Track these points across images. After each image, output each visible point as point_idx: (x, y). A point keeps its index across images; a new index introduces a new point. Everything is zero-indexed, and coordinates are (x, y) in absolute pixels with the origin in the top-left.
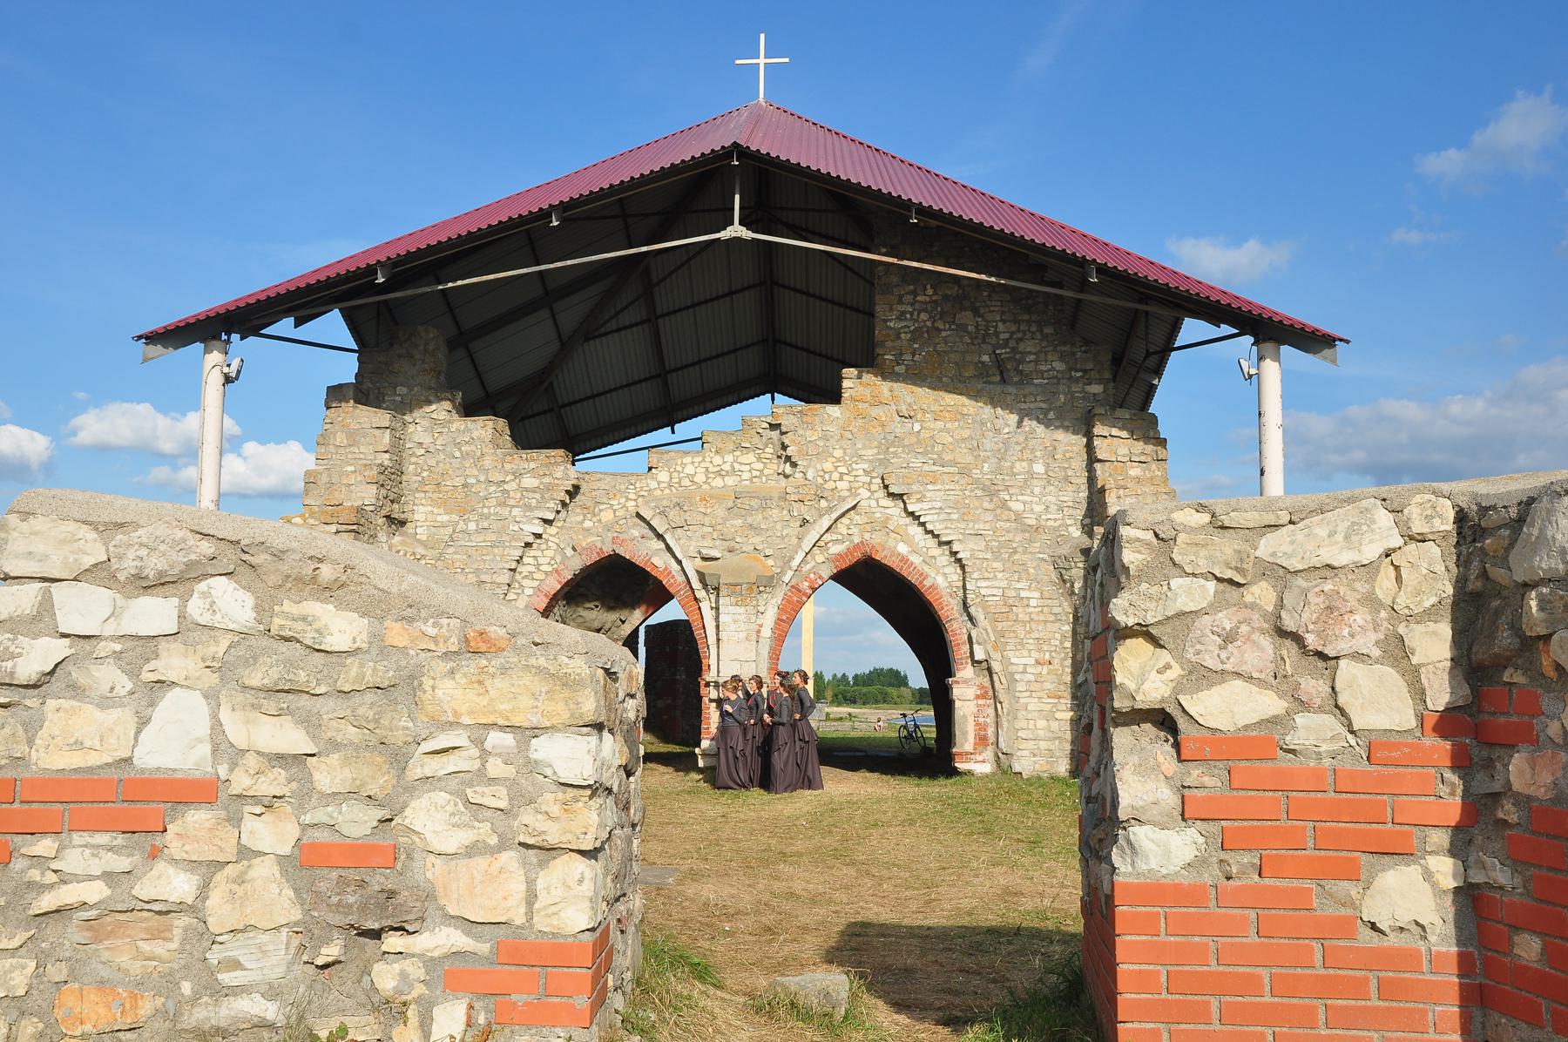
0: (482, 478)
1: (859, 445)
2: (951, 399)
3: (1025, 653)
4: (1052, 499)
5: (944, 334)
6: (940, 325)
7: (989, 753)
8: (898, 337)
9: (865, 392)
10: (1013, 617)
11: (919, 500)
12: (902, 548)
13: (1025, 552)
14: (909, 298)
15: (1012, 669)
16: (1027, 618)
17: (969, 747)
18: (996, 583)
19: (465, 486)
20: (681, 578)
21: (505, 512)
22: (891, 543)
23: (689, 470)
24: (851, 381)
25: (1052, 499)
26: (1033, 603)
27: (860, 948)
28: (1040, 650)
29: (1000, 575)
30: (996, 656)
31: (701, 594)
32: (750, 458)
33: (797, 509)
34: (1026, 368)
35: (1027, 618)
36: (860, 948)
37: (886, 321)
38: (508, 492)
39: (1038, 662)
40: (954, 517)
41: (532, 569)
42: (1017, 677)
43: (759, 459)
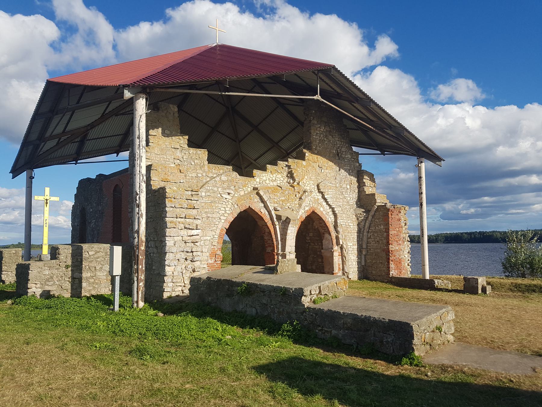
2: (331, 163)
9: (311, 158)
12: (322, 209)
19: (197, 177)
21: (215, 189)
22: (319, 207)
23: (264, 178)
27: (260, 369)
30: (345, 243)
32: (279, 176)
34: (343, 156)
36: (260, 369)
41: (223, 212)
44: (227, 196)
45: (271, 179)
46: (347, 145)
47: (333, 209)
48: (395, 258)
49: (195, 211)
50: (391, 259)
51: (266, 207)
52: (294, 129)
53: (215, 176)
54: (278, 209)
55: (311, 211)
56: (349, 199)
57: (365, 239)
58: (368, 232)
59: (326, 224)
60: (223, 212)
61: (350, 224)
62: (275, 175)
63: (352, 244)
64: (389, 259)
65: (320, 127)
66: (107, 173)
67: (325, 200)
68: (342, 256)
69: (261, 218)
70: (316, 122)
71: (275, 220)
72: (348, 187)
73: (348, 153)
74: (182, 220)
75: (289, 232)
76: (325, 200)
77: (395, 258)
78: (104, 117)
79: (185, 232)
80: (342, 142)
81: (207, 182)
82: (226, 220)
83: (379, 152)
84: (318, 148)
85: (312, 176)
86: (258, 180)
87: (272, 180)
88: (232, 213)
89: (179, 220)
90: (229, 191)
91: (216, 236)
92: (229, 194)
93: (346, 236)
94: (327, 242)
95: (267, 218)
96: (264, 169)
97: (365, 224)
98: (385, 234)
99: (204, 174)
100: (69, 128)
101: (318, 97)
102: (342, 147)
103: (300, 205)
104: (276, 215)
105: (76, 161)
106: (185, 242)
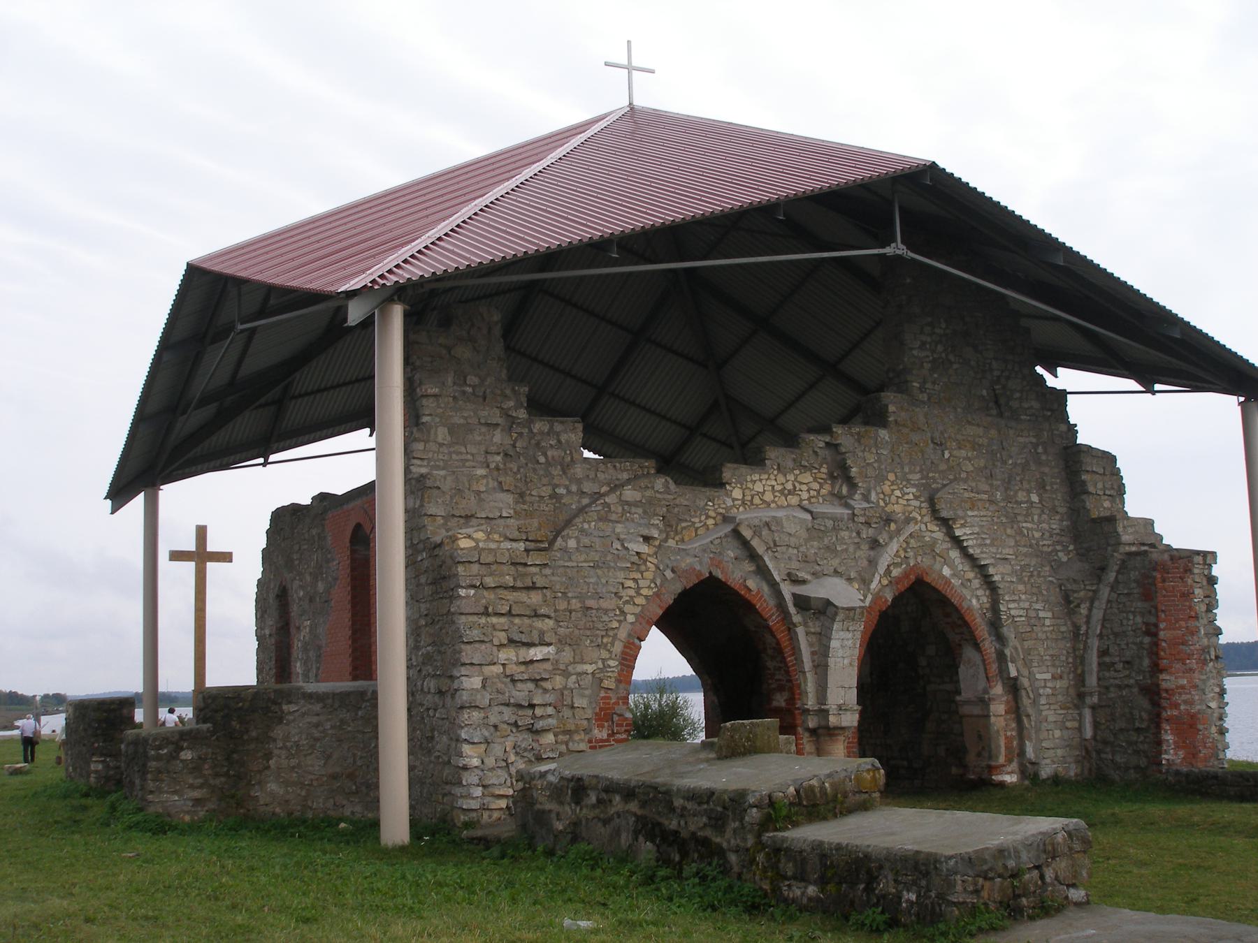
0: (574, 488)
1: (906, 469)
3: (1044, 669)
4: (1045, 526)
5: (955, 366)
6: (952, 357)
7: (1014, 766)
8: (922, 366)
10: (1034, 635)
11: (963, 526)
12: (946, 571)
13: (1039, 576)
14: (928, 329)
15: (1037, 684)
16: (1044, 637)
17: (1002, 760)
18: (1022, 605)
20: (772, 603)
23: (759, 487)
24: (893, 403)
25: (1045, 526)
26: (1047, 622)
28: (1053, 666)
29: (1023, 597)
31: (797, 619)
32: (807, 477)
33: (867, 533)
34: (1015, 404)
35: (1044, 637)
37: (912, 349)
38: (608, 505)
39: (1054, 678)
40: (988, 542)
41: (632, 592)
42: (1041, 691)
43: (815, 479)
44: (644, 549)
45: (778, 488)
47: (981, 570)
49: (535, 598)
50: (1164, 714)
51: (762, 571)
53: (604, 489)
54: (802, 575)
55: (912, 577)
56: (1037, 535)
59: (962, 618)
60: (632, 592)
61: (1041, 614)
63: (1048, 676)
64: (1158, 715)
66: (340, 489)
67: (957, 542)
68: (1016, 711)
69: (749, 606)
71: (792, 610)
72: (1035, 498)
74: (502, 620)
75: (834, 644)
77: (1175, 713)
81: (582, 510)
83: (1132, 384)
84: (928, 385)
85: (911, 472)
86: (737, 494)
87: (781, 492)
88: (657, 595)
89: (494, 620)
90: (646, 532)
91: (612, 663)
92: (647, 539)
93: (1028, 652)
98: (1147, 640)
99: (574, 488)
100: (246, 370)
101: (896, 248)
102: (1008, 378)
103: (873, 563)
104: (794, 595)
105: (266, 460)
106: (514, 681)
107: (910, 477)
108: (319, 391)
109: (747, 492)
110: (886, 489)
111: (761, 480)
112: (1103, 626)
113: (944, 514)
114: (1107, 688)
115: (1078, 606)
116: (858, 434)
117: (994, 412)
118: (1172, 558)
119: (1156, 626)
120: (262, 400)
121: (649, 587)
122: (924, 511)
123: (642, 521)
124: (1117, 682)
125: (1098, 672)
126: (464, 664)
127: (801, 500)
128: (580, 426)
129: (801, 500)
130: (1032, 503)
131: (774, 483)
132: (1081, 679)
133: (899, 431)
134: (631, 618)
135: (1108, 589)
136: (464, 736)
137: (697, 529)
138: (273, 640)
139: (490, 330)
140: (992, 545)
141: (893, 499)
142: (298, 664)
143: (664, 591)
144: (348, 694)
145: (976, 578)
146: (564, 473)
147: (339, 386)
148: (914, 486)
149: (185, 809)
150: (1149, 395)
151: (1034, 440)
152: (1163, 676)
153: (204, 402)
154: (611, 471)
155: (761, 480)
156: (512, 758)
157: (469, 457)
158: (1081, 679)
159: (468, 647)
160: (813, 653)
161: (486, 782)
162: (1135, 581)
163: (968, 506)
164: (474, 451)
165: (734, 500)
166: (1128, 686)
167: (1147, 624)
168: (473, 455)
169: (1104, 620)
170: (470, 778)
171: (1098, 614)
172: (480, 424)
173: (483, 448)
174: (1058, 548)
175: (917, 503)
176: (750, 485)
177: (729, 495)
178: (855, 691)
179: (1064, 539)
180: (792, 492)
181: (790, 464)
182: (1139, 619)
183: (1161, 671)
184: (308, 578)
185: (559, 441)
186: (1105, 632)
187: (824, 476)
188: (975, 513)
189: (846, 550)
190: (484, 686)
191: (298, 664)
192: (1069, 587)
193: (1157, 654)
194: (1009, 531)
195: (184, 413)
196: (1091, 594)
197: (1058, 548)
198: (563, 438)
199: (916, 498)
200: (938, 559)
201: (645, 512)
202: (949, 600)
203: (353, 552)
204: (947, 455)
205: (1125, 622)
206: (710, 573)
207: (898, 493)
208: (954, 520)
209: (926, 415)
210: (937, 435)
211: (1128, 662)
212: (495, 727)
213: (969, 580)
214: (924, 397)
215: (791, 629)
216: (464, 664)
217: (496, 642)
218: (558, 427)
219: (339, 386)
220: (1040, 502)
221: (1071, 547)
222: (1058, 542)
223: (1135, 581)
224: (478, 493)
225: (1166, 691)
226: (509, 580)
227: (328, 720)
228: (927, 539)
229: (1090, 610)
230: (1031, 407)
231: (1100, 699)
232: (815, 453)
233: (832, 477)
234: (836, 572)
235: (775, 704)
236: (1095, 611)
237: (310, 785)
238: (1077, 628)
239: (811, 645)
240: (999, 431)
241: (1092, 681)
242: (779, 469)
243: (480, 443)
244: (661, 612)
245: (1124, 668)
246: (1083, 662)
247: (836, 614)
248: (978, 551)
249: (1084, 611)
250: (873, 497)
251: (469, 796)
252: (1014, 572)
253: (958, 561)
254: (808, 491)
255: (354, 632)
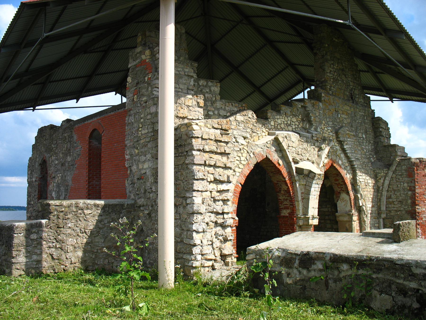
0: (216, 112)
1: (328, 120)
6: (339, 78)
11: (347, 144)
14: (332, 66)
23: (279, 121)
25: (367, 147)
31: (297, 178)
32: (294, 120)
37: (327, 73)
40: (353, 151)
45: (285, 122)
46: (359, 88)
48: (421, 221)
52: (281, 71)
57: (384, 199)
58: (388, 191)
62: (289, 119)
65: (333, 64)
67: (344, 150)
70: (329, 57)
72: (364, 136)
73: (361, 97)
75: (312, 189)
76: (344, 150)
77: (421, 221)
78: (72, 53)
79: (213, 186)
80: (354, 83)
82: (241, 173)
83: (388, 99)
84: (332, 88)
86: (272, 123)
87: (286, 124)
88: (248, 164)
90: (245, 135)
92: (245, 138)
94: (343, 203)
95: (284, 172)
96: (278, 112)
97: (384, 181)
98: (410, 193)
99: (216, 112)
100: (32, 67)
102: (355, 89)
107: (329, 123)
108: (61, 80)
109: (276, 123)
110: (323, 127)
111: (280, 118)
112: (389, 187)
113: (341, 139)
114: (390, 211)
115: (380, 179)
116: (313, 103)
117: (351, 101)
118: (420, 161)
119: (414, 187)
120: (34, 83)
121: (244, 160)
122: (334, 137)
123: (244, 130)
124: (395, 209)
125: (386, 205)
126: (195, 191)
127: (293, 129)
128: (219, 85)
129: (293, 129)
130: (364, 138)
131: (284, 120)
132: (379, 208)
133: (325, 104)
134: (238, 174)
135: (392, 173)
136: (194, 228)
137: (259, 137)
138: (37, 183)
139: (181, 36)
140: (354, 153)
141: (325, 131)
142: (54, 193)
143: (250, 163)
144: (116, 205)
145: (348, 166)
146: (212, 105)
147: (68, 79)
148: (330, 127)
149: (32, 266)
150: (390, 102)
151: (363, 114)
152: (417, 207)
153: (15, 78)
154: (231, 106)
155: (280, 118)
156: (215, 240)
157: (180, 90)
158: (379, 208)
159: (196, 181)
160: (302, 193)
161: (204, 252)
162: (404, 170)
163: (348, 136)
164: (182, 88)
165: (271, 126)
166: (400, 210)
167: (410, 187)
168: (182, 89)
169: (389, 185)
170: (196, 250)
171: (387, 182)
172: (185, 75)
173: (186, 87)
174: (371, 156)
175: (331, 134)
176: (276, 120)
177: (269, 123)
178: (317, 209)
179: (372, 153)
180: (290, 125)
181: (289, 113)
182: (406, 185)
183: (416, 205)
184: (61, 155)
185: (210, 91)
186: (389, 189)
187: (300, 120)
188: (350, 140)
189: (311, 150)
190: (203, 203)
191: (54, 193)
192: (377, 171)
193: (415, 198)
194: (359, 148)
195: (5, 81)
196: (384, 174)
197: (371, 156)
198: (212, 89)
199: (331, 132)
200: (338, 157)
201: (245, 126)
202: (341, 174)
203: (90, 142)
204: (339, 116)
205: (399, 186)
206: (266, 156)
207: (326, 129)
208: (344, 142)
209: (333, 99)
210: (337, 108)
211: (400, 201)
212: (207, 223)
213: (346, 167)
214: (331, 92)
215: (293, 183)
216: (195, 191)
217: (209, 180)
218: (210, 84)
219: (68, 79)
220: (366, 138)
221: (375, 156)
222: (370, 154)
223: (404, 170)
224: (188, 106)
225: (418, 213)
226: (214, 148)
227: (106, 218)
228: (335, 149)
229: (384, 181)
230: (361, 102)
231: (386, 216)
232: (298, 109)
233: (303, 120)
234: (308, 159)
235: (282, 214)
236: (386, 181)
237: (97, 252)
238: (379, 187)
239: (301, 190)
240: (354, 109)
241: (383, 208)
242: (285, 114)
243: (185, 84)
244: (249, 172)
245: (398, 203)
246: (380, 200)
247: (315, 176)
248: (351, 155)
249: (382, 181)
250: (319, 130)
251: (196, 260)
252: (361, 164)
253: (343, 158)
254: (295, 125)
255: (89, 178)
